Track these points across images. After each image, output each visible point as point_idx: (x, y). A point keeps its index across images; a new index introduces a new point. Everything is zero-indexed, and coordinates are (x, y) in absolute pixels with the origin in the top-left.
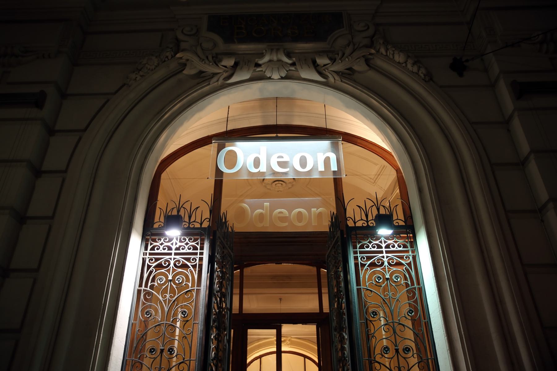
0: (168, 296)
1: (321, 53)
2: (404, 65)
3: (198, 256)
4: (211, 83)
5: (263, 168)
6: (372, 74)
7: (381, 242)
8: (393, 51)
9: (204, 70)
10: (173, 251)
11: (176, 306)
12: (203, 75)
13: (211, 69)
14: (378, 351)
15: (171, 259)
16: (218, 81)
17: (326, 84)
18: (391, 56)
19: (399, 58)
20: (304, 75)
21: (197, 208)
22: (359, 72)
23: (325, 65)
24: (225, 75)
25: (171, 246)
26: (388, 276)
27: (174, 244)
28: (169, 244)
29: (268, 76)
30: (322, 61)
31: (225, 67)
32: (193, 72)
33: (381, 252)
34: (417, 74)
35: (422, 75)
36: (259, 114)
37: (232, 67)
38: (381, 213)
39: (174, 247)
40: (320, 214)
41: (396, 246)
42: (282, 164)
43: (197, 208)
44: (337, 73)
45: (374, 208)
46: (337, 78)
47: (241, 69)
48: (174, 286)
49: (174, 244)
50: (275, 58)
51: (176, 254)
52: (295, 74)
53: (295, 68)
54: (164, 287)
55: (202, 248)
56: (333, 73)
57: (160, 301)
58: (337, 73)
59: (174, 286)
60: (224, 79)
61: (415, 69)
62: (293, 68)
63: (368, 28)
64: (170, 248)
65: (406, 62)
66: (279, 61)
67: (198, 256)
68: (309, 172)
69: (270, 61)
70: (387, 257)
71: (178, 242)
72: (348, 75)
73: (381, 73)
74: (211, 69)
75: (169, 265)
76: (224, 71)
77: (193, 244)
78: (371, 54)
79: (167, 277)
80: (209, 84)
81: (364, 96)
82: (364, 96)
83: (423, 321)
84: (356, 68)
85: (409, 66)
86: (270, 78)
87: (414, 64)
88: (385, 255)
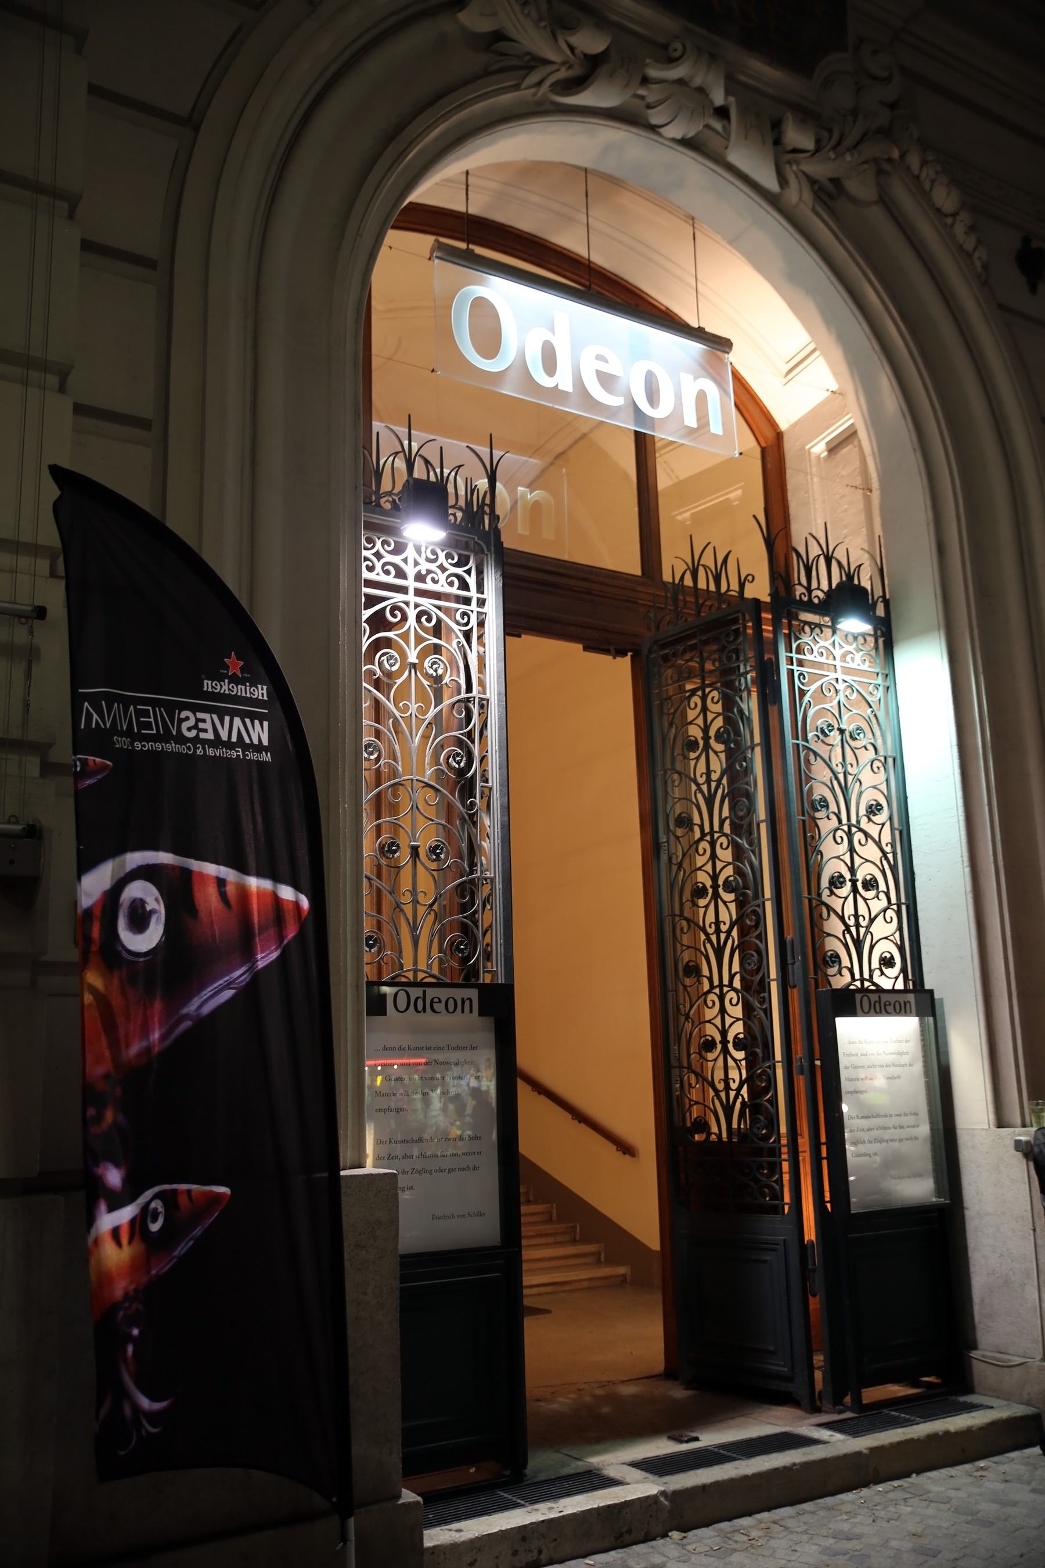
0: (413, 707)
1: (807, 115)
2: (949, 221)
3: (795, 667)
4: (524, 85)
5: (563, 380)
6: (877, 216)
7: (405, 560)
8: (937, 173)
9: (512, 33)
10: (794, 655)
11: (389, 731)
12: (501, 45)
13: (532, 38)
14: (825, 883)
15: (407, 604)
16: (539, 84)
17: (773, 200)
18: (927, 186)
19: (945, 198)
20: (737, 157)
21: (459, 467)
22: (853, 200)
23: (796, 151)
24: (563, 74)
25: (402, 565)
26: (413, 658)
27: (411, 562)
28: (397, 559)
29: (654, 121)
30: (797, 137)
31: (572, 49)
32: (484, 26)
33: (404, 590)
34: (969, 255)
35: (978, 264)
36: (494, 185)
37: (585, 55)
38: (416, 475)
39: (411, 571)
40: (536, 504)
41: (378, 565)
42: (606, 380)
43: (459, 467)
44: (812, 181)
45: (400, 464)
46: (808, 196)
47: (611, 75)
48: (426, 683)
49: (411, 562)
50: (698, 81)
51: (419, 593)
52: (715, 143)
53: (724, 127)
54: (399, 681)
55: (480, 588)
56: (803, 180)
57: (396, 718)
58: (812, 181)
59: (426, 683)
60: (551, 85)
61: (969, 244)
62: (718, 126)
63: (888, 80)
64: (401, 574)
65: (954, 215)
66: (701, 90)
67: (795, 667)
68: (498, 377)
69: (681, 82)
70: (416, 606)
71: (422, 560)
72: (829, 195)
73: (896, 220)
74: (532, 38)
75: (405, 618)
76: (563, 63)
77: (460, 571)
78: (890, 160)
79: (403, 655)
80: (517, 87)
81: (853, 270)
82: (853, 270)
83: (479, 784)
84: (853, 186)
85: (959, 230)
86: (654, 129)
87: (972, 229)
88: (411, 597)
